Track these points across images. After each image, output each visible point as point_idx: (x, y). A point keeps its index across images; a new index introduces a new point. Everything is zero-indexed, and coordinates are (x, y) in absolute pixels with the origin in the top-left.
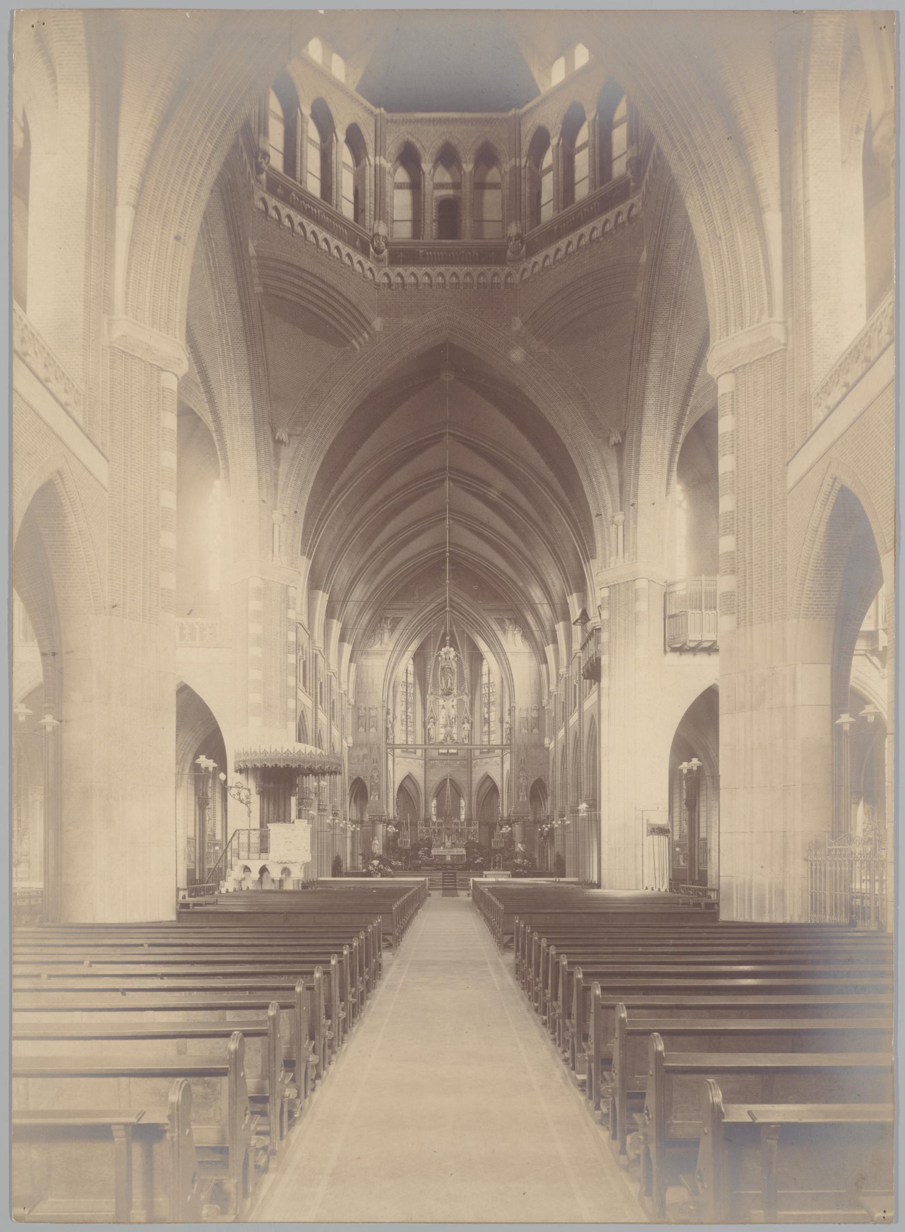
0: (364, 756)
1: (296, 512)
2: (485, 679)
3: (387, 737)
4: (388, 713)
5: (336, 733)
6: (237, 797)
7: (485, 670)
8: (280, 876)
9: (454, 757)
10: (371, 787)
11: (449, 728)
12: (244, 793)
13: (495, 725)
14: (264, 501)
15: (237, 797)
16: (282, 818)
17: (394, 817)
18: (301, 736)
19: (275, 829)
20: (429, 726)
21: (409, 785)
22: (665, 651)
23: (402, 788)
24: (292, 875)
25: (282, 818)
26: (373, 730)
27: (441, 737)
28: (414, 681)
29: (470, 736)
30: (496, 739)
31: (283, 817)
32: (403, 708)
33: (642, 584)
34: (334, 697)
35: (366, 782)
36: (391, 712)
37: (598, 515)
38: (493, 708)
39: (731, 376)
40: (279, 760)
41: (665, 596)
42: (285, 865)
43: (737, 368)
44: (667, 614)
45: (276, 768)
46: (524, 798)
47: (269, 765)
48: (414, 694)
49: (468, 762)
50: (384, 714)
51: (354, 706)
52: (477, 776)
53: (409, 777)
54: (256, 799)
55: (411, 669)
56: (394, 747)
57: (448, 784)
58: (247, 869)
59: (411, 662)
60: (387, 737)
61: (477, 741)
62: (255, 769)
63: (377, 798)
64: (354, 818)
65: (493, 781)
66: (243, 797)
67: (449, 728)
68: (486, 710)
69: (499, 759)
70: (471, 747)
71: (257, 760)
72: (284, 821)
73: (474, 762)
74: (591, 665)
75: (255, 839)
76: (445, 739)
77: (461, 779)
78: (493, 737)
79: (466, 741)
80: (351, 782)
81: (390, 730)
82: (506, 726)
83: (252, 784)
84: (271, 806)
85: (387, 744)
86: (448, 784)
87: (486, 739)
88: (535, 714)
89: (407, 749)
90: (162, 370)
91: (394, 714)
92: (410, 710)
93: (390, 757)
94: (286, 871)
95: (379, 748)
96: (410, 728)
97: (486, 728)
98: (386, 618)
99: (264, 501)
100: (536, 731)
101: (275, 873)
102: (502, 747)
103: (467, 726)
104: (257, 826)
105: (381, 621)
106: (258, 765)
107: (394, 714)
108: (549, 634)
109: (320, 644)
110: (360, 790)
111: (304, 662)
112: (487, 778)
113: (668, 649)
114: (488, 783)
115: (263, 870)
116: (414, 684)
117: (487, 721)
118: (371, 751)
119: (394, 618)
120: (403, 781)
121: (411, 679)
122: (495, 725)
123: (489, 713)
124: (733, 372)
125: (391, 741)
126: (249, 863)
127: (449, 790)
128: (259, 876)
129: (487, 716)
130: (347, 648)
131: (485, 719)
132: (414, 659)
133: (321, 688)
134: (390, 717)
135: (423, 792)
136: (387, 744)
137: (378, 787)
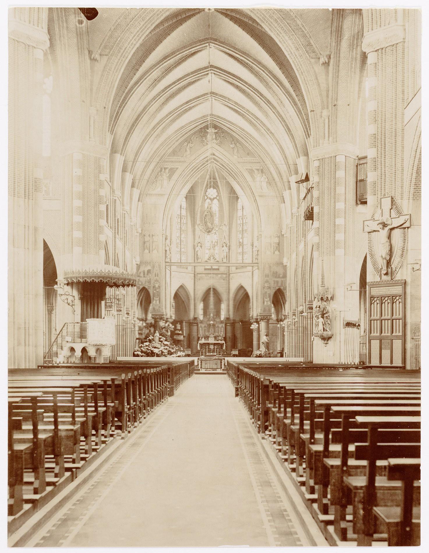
0: (149, 271)
1: (105, 108)
2: (240, 213)
3: (166, 257)
4: (166, 239)
5: (128, 254)
6: (66, 301)
7: (239, 206)
8: (95, 354)
9: (215, 272)
10: (154, 294)
11: (212, 251)
12: (70, 299)
13: (248, 248)
14: (83, 101)
15: (66, 301)
16: (96, 315)
17: (171, 317)
18: (107, 262)
19: (91, 323)
20: (197, 249)
21: (182, 294)
22: (357, 204)
23: (176, 296)
24: (103, 354)
25: (96, 315)
26: (155, 252)
27: (207, 257)
28: (187, 207)
29: (228, 257)
30: (248, 259)
31: (96, 315)
32: (178, 234)
33: (341, 159)
34: (126, 228)
35: (149, 290)
36: (169, 238)
37: (311, 111)
38: (245, 235)
39: (376, 53)
40: (95, 277)
41: (357, 166)
42: (98, 347)
43: (378, 50)
44: (359, 179)
45: (93, 283)
46: (269, 302)
47: (89, 280)
48: (186, 223)
49: (228, 276)
50: (164, 239)
51: (141, 234)
52: (234, 287)
53: (182, 287)
54: (78, 303)
55: (184, 205)
56: (169, 264)
57: (212, 292)
58: (72, 350)
59: (184, 200)
60: (166, 257)
61: (233, 260)
62: (79, 283)
63: (158, 303)
64: (140, 317)
65: (245, 290)
66: (69, 301)
67: (212, 251)
68: (240, 236)
69: (250, 273)
70: (228, 265)
71: (80, 277)
72: (97, 317)
73: (231, 275)
74: (309, 211)
75: (77, 329)
76: (209, 259)
77: (221, 290)
78: (245, 257)
79: (225, 261)
80: (139, 290)
81: (168, 252)
82: (255, 249)
83: (75, 293)
84: (89, 307)
85: (166, 262)
86: (212, 292)
87: (240, 258)
88: (276, 240)
89: (180, 264)
90: (35, 48)
91: (171, 240)
92: (183, 236)
93: (168, 272)
94: (98, 351)
95: (159, 266)
96: (183, 250)
97: (240, 250)
98: (165, 169)
99: (83, 101)
100: (277, 253)
101: (92, 352)
102: (253, 264)
103: (226, 249)
104: (79, 321)
105: (161, 171)
106: (81, 280)
107: (171, 240)
108: (286, 184)
109: (118, 193)
110: (145, 298)
111: (107, 206)
112: (241, 287)
113: (358, 202)
114: (241, 292)
115: (84, 350)
116: (187, 216)
117: (241, 244)
118: (153, 267)
119: (171, 169)
120: (178, 290)
121: (184, 212)
122: (248, 248)
123: (242, 238)
124: (376, 51)
125: (168, 260)
126: (74, 346)
127: (212, 296)
128: (81, 354)
129: (241, 240)
130: (136, 192)
131: (240, 242)
132: (186, 198)
133: (118, 222)
134: (168, 241)
135: (193, 298)
136: (166, 262)
137: (159, 295)
